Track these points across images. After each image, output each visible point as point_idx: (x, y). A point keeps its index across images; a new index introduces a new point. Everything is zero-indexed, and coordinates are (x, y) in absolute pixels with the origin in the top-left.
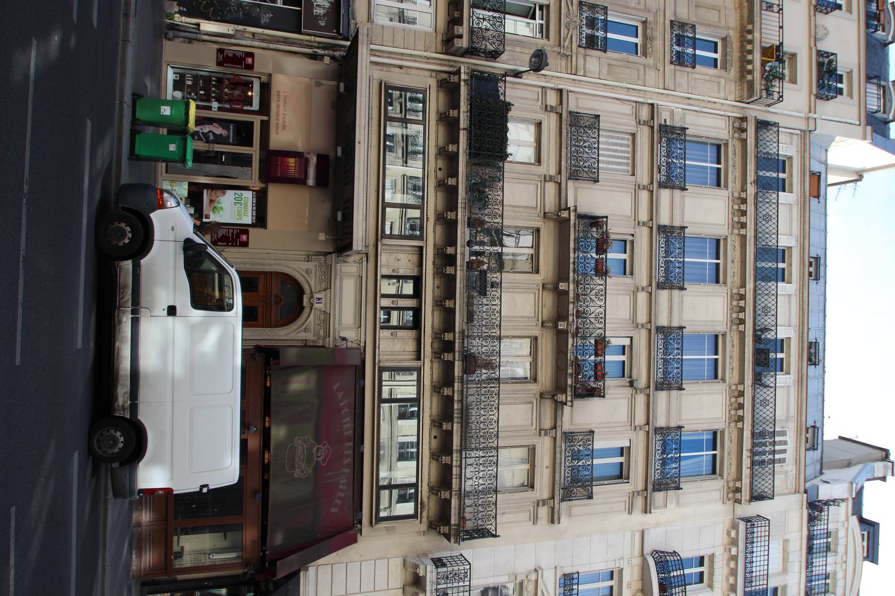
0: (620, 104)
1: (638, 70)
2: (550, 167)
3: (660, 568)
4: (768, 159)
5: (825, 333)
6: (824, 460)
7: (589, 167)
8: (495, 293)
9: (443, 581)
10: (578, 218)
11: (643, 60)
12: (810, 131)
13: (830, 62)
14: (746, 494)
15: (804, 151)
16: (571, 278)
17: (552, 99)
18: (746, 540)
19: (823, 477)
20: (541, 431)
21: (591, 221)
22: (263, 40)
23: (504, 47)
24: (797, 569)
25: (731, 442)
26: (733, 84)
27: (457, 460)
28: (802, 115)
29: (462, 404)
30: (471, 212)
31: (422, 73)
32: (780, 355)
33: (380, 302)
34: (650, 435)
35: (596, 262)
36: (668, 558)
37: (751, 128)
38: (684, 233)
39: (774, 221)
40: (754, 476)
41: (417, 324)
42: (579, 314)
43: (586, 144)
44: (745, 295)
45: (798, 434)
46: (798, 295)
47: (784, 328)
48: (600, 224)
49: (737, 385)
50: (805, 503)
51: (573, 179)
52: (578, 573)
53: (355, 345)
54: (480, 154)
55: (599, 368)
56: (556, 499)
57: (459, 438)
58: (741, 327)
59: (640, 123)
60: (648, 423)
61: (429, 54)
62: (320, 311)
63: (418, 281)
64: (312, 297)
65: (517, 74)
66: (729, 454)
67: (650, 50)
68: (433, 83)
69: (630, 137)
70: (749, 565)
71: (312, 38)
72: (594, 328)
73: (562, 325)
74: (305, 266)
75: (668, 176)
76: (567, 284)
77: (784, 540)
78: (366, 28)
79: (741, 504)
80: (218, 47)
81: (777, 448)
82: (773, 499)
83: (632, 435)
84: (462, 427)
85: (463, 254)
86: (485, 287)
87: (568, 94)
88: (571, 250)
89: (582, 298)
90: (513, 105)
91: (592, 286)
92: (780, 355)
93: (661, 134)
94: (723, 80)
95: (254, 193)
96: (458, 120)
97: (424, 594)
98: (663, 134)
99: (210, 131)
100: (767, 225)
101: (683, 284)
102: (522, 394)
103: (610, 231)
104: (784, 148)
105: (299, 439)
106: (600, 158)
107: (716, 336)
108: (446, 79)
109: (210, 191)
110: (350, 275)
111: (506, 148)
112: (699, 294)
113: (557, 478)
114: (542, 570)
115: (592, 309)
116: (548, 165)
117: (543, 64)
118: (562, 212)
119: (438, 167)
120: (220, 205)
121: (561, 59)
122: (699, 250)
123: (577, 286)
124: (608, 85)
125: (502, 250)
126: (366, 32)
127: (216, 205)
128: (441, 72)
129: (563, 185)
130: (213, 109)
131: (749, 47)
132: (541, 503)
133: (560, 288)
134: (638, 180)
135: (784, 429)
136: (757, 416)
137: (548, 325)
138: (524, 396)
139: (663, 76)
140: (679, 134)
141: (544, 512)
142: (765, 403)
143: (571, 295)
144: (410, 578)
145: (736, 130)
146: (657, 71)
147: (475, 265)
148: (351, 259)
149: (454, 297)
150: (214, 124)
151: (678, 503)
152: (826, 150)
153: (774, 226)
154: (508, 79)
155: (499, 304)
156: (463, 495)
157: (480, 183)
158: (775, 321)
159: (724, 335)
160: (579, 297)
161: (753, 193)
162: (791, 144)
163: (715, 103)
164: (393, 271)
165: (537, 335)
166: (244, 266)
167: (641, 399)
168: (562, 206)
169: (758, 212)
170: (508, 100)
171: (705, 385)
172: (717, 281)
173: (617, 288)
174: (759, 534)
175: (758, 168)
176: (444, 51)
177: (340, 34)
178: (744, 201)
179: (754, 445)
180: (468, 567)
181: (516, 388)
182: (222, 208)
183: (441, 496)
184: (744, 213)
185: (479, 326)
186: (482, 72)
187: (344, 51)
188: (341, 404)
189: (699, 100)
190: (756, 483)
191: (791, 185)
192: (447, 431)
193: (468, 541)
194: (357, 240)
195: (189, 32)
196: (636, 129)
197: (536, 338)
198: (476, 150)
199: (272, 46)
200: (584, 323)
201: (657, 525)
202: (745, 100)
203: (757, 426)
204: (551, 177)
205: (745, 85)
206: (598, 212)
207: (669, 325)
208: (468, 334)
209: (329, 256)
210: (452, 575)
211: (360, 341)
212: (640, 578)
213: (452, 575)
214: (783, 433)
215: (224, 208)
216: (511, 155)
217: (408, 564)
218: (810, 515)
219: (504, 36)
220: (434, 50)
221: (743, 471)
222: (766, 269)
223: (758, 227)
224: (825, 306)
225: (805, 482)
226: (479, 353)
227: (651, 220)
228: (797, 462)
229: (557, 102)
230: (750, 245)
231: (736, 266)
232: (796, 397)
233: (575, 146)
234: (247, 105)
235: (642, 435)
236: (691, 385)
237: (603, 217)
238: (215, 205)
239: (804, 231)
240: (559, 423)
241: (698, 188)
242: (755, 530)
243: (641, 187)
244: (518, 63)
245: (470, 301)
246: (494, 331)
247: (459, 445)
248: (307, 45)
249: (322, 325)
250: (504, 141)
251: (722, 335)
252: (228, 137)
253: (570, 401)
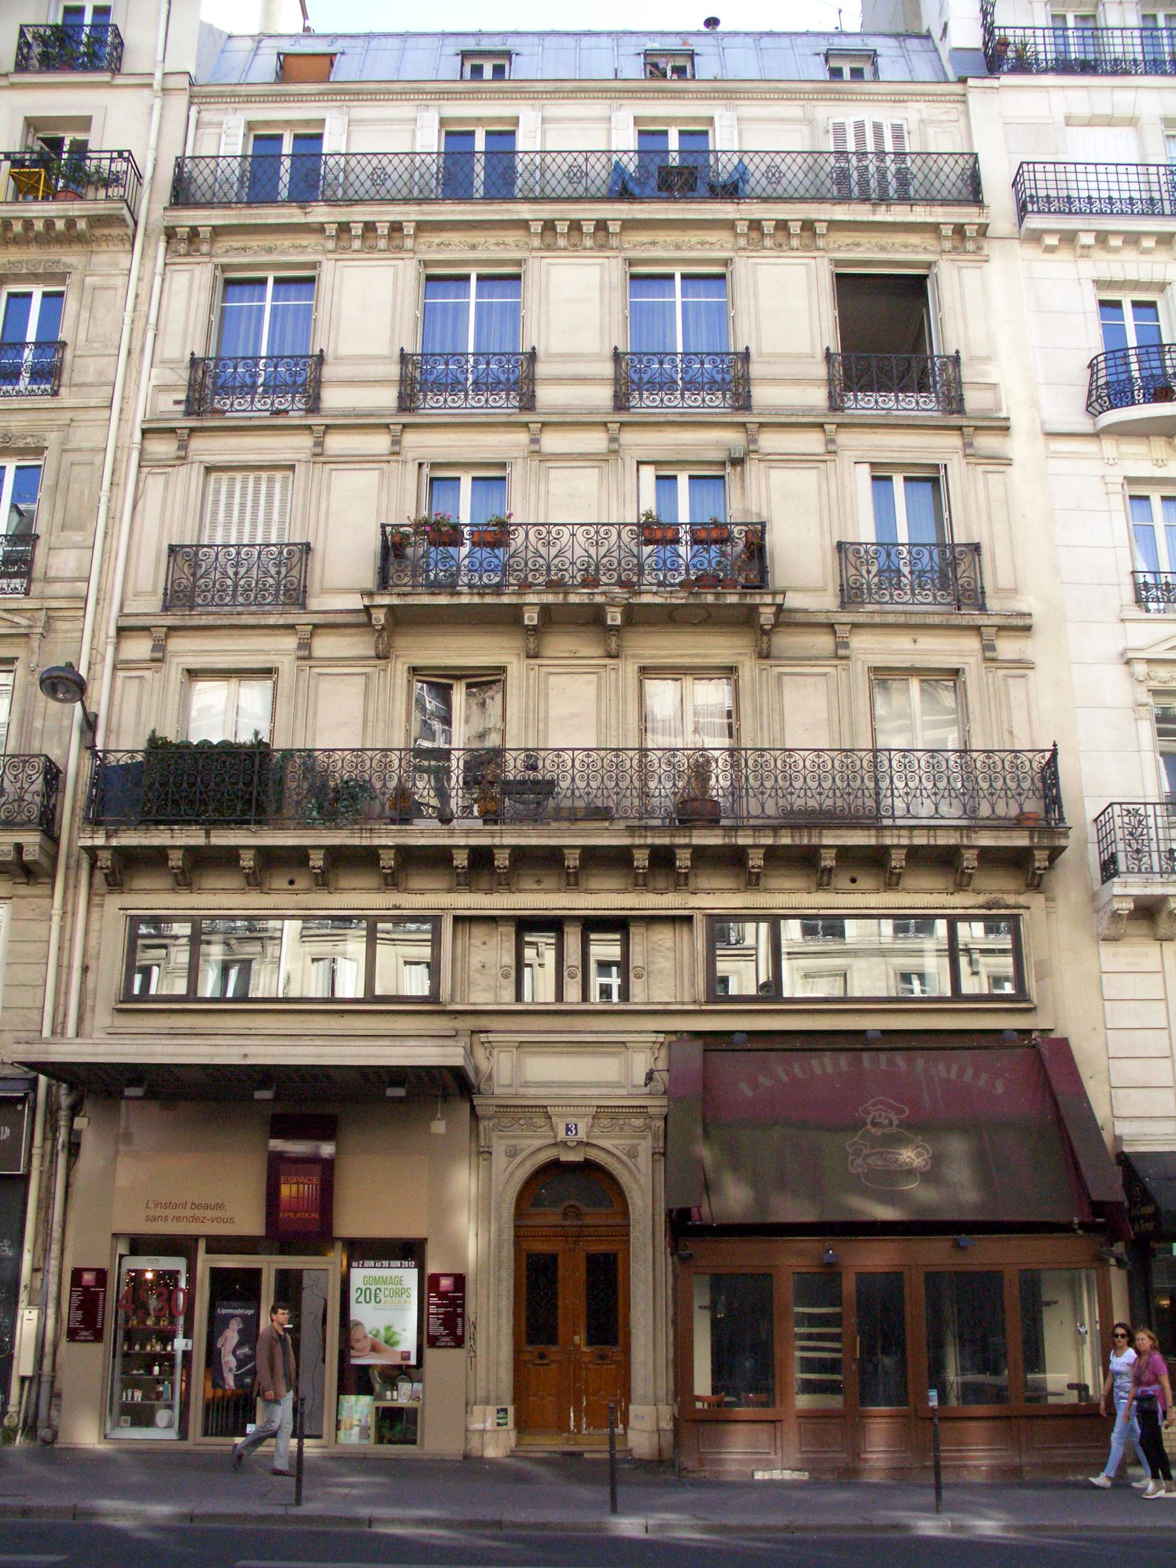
0: (145, 501)
1: (72, 464)
2: (282, 647)
3: (1121, 399)
4: (254, 179)
5: (625, 33)
6: (901, 30)
7: (278, 565)
8: (548, 762)
9: (1144, 860)
10: (385, 588)
11: (51, 456)
12: (191, 84)
13: (38, 37)
14: (968, 215)
15: (234, 96)
16: (514, 600)
17: (139, 648)
18: (1063, 212)
19: (936, 34)
20: (840, 654)
21: (392, 558)
22: (45, 1250)
23: (37, 756)
24: (1129, 96)
25: (858, 245)
26: (96, 259)
27: (899, 836)
28: (158, 103)
29: (782, 827)
30: (380, 817)
31: (95, 926)
32: (674, 143)
33: (572, 1003)
34: (846, 421)
35: (479, 545)
36: (1101, 382)
37: (189, 217)
38: (413, 355)
39: (385, 161)
40: (928, 197)
41: (619, 925)
42: (590, 582)
43: (231, 572)
44: (545, 221)
45: (840, 97)
46: (543, 102)
47: (613, 132)
48: (397, 539)
49: (736, 235)
50: (988, 82)
51: (304, 598)
52: (1133, 572)
53: (663, 1053)
54: (257, 800)
55: (703, 535)
56: (980, 623)
57: (853, 832)
58: (614, 227)
59: (184, 458)
60: (821, 426)
61: (56, 912)
62: (592, 1126)
63: (526, 925)
64: (564, 1143)
65: (90, 724)
66: (883, 249)
67: (29, 440)
68: (114, 902)
69: (213, 476)
70: (1117, 207)
71: (36, 1151)
72: (619, 547)
73: (614, 617)
74: (500, 1160)
75: (292, 388)
76: (525, 608)
77: (1067, 125)
78: (15, 1046)
79: (988, 225)
80: (64, 1339)
81: (870, 147)
82: (976, 154)
83: (846, 458)
84: (829, 828)
85: (468, 833)
86: (536, 782)
87: (127, 615)
88: (455, 600)
89: (556, 574)
90: (154, 732)
91: (530, 554)
92: (674, 143)
93: (205, 412)
94: (88, 280)
95: (355, 1264)
96: (188, 850)
97: (1171, 900)
98: (206, 406)
99: (234, 1353)
100: (395, 177)
101: (523, 354)
102: (761, 697)
103: (413, 517)
104: (230, 140)
105: (852, 1161)
106: (259, 541)
107: (634, 277)
108: (106, 875)
109: (353, 1352)
110: (517, 1068)
111: (241, 746)
112: (543, 318)
113: (937, 620)
114: (1126, 650)
115: (579, 552)
116: (277, 652)
117: (70, 676)
118: (374, 622)
119: (287, 886)
120: (382, 1332)
121: (55, 631)
122: (450, 325)
123: (531, 585)
124: (106, 527)
125: (459, 749)
126: (22, 1047)
127: (381, 1339)
128: (91, 885)
129: (317, 619)
130: (190, 1348)
131: (18, 227)
132: (989, 654)
133: (535, 622)
134: (302, 456)
135: (831, 128)
136: (802, 191)
137: (614, 646)
138: (765, 693)
139: (82, 412)
140: (204, 373)
141: (1007, 648)
142: (774, 175)
143: (549, 599)
144: (1141, 927)
145: (194, 247)
146: (74, 424)
147: (491, 806)
148: (484, 1065)
149: (560, 849)
150: (219, 1345)
151: (988, 359)
152: (230, 37)
153: (396, 161)
154: (99, 746)
155: (570, 753)
156: (973, 823)
157: (317, 798)
158: (598, 155)
159: (631, 262)
160: (551, 581)
161: (326, 209)
162: (220, 124)
163: (137, 296)
164: (506, 976)
165: (636, 667)
166: (504, 1283)
167: (770, 441)
168: (361, 621)
169: (367, 197)
170: (142, 745)
171: (738, 302)
172: (517, 277)
173: (533, 497)
174: (1129, 41)
175: (269, 199)
176: (48, 880)
177: (26, 1095)
178: (344, 228)
179: (865, 199)
180: (1117, 808)
181: (750, 712)
182: (388, 1328)
183: (973, 868)
184: (370, 227)
185: (617, 794)
186: (91, 801)
187: (59, 1087)
188: (785, 1079)
189: (132, 330)
190: (944, 193)
191: (307, 123)
192: (838, 858)
193: (1064, 809)
194: (445, 1056)
195: (38, 1396)
196: (196, 466)
197: (643, 670)
198: (250, 809)
199: (56, 1234)
200: (609, 570)
201: (1034, 404)
202: (130, 232)
203: (824, 191)
204: (301, 646)
205: (99, 232)
206: (373, 543)
207: (611, 382)
208: (635, 818)
209: (479, 1111)
210: (1133, 842)
211: (654, 1042)
212: (1144, 440)
213: (1133, 842)
214: (840, 129)
215: (387, 1324)
216: (256, 733)
217: (1112, 932)
218: (1014, 70)
219: (13, 756)
220: (45, 902)
221: (919, 220)
222: (487, 176)
223: (399, 197)
224: (568, 34)
225: (947, 82)
226: (675, 794)
227: (387, 426)
228: (899, 99)
229: (144, 637)
230: (439, 213)
231: (482, 240)
232: (761, 102)
233: (234, 596)
234: (177, 1282)
235: (844, 438)
236: (739, 333)
237: (384, 534)
238: (382, 1342)
239: (406, 93)
240: (822, 619)
241: (319, 325)
242: (1042, 193)
243: (318, 450)
244: (66, 723)
245: (565, 814)
246: (628, 763)
247: (866, 833)
248: (51, 1162)
249: (621, 1122)
250: (228, 750)
251: (630, 265)
252: (243, 1317)
253: (774, 598)
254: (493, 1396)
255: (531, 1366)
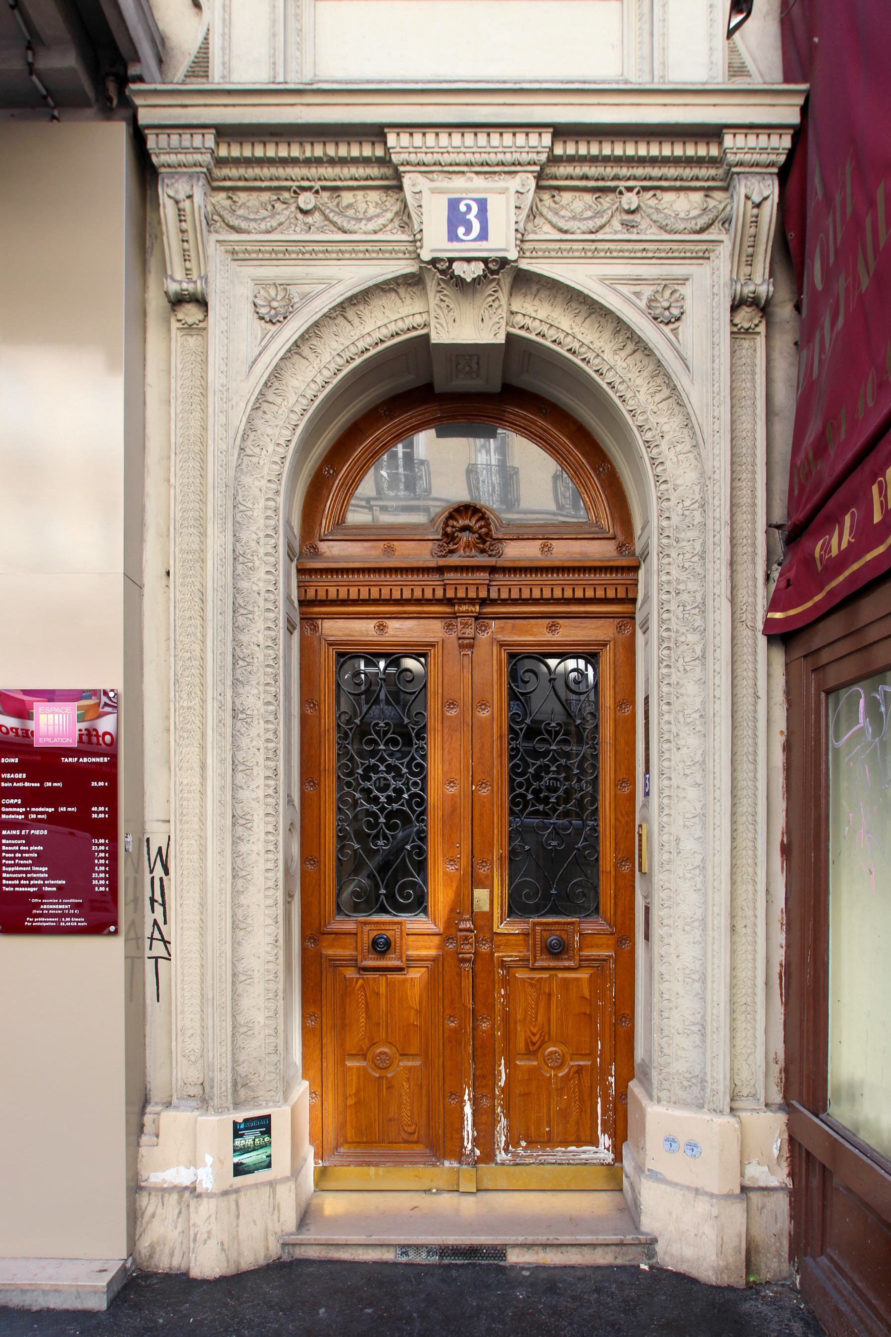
62: (533, 214)
166: (258, 728)
249: (630, 200)
254: (223, 1079)
255: (351, 973)
